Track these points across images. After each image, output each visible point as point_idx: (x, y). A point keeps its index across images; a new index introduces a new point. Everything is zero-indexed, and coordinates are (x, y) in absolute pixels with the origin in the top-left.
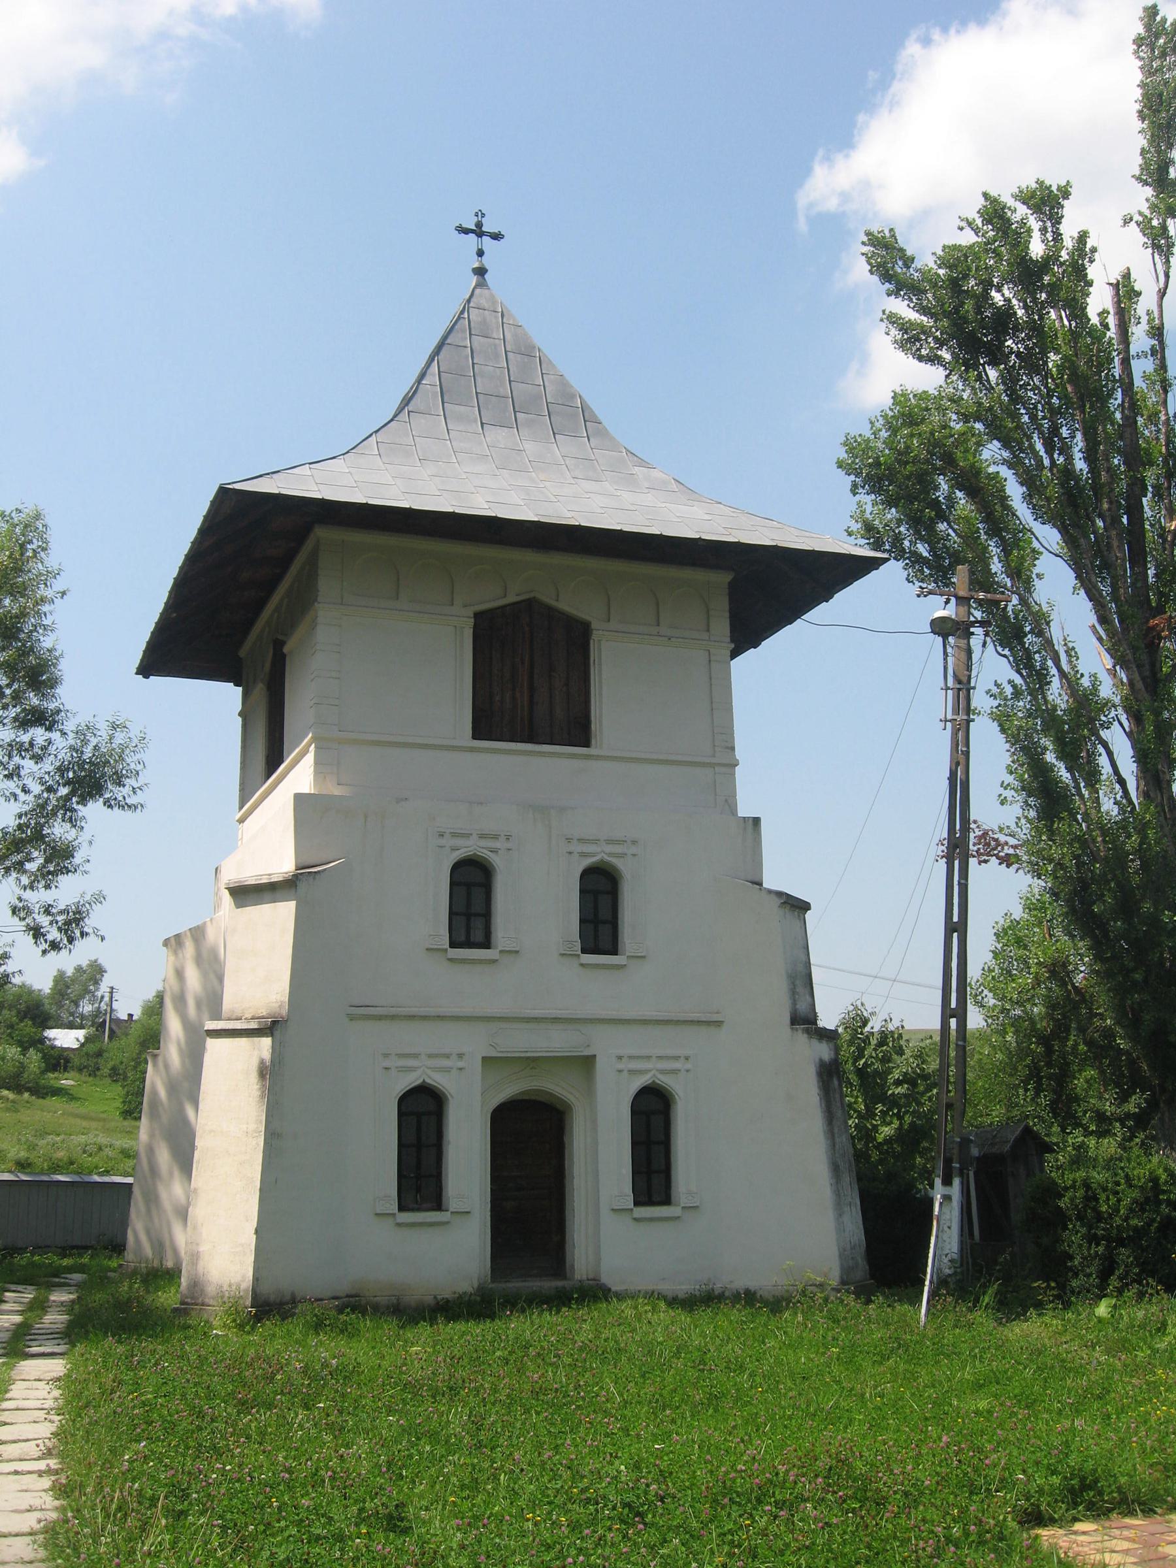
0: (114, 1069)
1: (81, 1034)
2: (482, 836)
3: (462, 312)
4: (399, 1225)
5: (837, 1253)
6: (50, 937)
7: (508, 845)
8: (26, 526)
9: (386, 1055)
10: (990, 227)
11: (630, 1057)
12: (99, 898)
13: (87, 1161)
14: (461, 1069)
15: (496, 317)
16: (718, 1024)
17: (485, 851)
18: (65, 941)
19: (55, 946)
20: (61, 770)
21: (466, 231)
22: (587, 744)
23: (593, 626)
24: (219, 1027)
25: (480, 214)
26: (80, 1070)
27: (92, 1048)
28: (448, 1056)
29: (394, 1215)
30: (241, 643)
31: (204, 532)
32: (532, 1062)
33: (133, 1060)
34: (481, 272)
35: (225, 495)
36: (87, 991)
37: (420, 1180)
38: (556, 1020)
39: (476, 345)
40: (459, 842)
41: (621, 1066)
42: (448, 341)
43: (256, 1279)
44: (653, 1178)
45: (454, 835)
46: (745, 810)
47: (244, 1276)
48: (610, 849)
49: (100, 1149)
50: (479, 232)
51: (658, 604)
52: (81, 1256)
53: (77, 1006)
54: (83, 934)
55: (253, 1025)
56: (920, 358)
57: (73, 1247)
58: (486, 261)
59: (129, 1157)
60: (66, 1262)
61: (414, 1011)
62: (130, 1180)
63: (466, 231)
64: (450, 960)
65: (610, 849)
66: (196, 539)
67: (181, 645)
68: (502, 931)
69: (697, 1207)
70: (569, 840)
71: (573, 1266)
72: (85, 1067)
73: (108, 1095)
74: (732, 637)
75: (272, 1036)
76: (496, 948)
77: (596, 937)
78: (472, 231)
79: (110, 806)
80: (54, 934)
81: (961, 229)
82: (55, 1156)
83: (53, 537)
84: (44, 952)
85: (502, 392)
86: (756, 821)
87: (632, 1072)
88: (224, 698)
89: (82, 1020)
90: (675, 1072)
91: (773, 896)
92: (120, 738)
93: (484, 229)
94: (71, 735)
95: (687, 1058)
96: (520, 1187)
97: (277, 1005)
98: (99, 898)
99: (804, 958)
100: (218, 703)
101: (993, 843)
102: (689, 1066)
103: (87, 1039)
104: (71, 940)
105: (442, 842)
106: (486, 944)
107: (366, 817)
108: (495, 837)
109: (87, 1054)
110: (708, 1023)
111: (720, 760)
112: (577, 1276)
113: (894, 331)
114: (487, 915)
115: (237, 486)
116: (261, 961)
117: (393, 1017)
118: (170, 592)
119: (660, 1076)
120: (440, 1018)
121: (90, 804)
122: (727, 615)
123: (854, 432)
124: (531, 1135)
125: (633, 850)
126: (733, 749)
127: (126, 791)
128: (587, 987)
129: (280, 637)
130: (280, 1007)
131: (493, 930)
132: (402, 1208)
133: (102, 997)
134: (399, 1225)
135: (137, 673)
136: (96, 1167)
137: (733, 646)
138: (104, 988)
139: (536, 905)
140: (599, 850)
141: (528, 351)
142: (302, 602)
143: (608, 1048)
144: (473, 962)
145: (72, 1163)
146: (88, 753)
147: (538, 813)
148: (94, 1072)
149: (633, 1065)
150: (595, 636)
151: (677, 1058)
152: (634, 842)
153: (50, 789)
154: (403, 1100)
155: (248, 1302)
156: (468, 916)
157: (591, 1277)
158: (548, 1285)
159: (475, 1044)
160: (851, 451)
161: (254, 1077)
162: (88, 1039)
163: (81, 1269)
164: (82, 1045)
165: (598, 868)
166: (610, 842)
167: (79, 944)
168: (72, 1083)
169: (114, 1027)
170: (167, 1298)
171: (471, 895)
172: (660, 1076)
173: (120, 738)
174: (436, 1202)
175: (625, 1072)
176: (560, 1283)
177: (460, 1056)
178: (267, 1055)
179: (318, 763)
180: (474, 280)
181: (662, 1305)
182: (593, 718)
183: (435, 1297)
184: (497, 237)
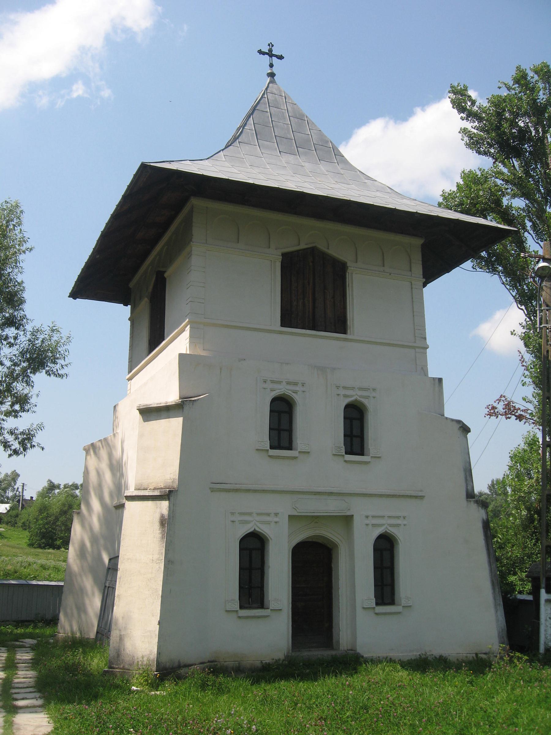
0: (23, 523)
1: (8, 506)
2: (288, 383)
3: (264, 94)
4: (240, 617)
5: (497, 634)
6: (13, 448)
7: (304, 389)
8: (11, 210)
9: (233, 514)
10: (517, 85)
11: (389, 517)
12: (41, 427)
13: (26, 571)
14: (276, 522)
15: (282, 99)
16: (421, 497)
17: (290, 392)
18: (22, 450)
19: (16, 452)
20: (22, 353)
22: (345, 332)
23: (348, 265)
24: (141, 494)
25: (271, 45)
26: (7, 523)
27: (14, 513)
28: (268, 515)
29: (237, 611)
30: (130, 280)
31: (125, 198)
32: (315, 519)
33: (35, 519)
34: (272, 75)
36: (10, 485)
37: (252, 591)
38: (331, 494)
39: (272, 112)
40: (276, 386)
41: (367, 522)
42: (257, 108)
43: (159, 653)
44: (385, 589)
45: (273, 382)
46: (433, 373)
47: (151, 651)
48: (360, 393)
49: (30, 565)
50: (270, 54)
52: (27, 627)
53: (5, 492)
54: (33, 446)
55: (157, 493)
56: (479, 153)
57: (23, 621)
58: (274, 70)
59: (45, 569)
60: (20, 631)
61: (250, 487)
62: (62, 584)
63: (263, 53)
64: (270, 456)
65: (360, 393)
66: (120, 202)
67: (100, 279)
69: (410, 606)
70: (338, 387)
71: (338, 642)
72: (10, 522)
73: (21, 536)
74: (423, 274)
75: (169, 500)
76: (297, 450)
77: (352, 445)
78: (266, 54)
79: (50, 375)
80: (16, 445)
81: (500, 88)
82: (6, 568)
83: (25, 218)
84: (10, 455)
85: (289, 136)
86: (440, 380)
87: (373, 525)
88: (122, 312)
89: (8, 499)
90: (398, 525)
92: (55, 338)
94: (28, 333)
95: (404, 518)
96: (303, 592)
97: (171, 481)
98: (41, 427)
99: (468, 460)
100: (114, 319)
101: (512, 409)
102: (405, 522)
103: (11, 508)
104: (25, 449)
105: (265, 386)
106: (290, 447)
107: (221, 369)
108: (296, 384)
109: (11, 516)
110: (416, 497)
111: (418, 345)
112: (341, 648)
113: (466, 139)
114: (290, 431)
115: (152, 164)
116: (154, 455)
117: (236, 490)
118: (98, 241)
119: (390, 528)
120: (264, 491)
121: (37, 374)
122: (421, 262)
123: (447, 190)
124: (315, 562)
126: (425, 339)
127: (58, 366)
128: (347, 475)
129: (162, 269)
130: (173, 482)
131: (294, 439)
132: (241, 607)
133: (18, 488)
134: (240, 617)
136: (29, 575)
137: (424, 280)
138: (19, 484)
139: (319, 425)
140: (354, 393)
141: (301, 117)
142: (181, 243)
143: (360, 510)
144: (284, 458)
145: (16, 572)
146: (38, 342)
148: (14, 524)
149: (375, 521)
150: (349, 271)
151: (398, 517)
152: (374, 390)
153: (15, 364)
154: (243, 540)
155: (154, 668)
157: (349, 648)
158: (326, 654)
159: (284, 507)
160: (445, 198)
161: (157, 525)
162: (12, 508)
163: (31, 636)
164: (8, 511)
165: (355, 406)
166: (361, 389)
167: (30, 452)
168: (3, 530)
169: (24, 503)
170: (96, 663)
171: (282, 418)
172: (390, 528)
173: (55, 338)
174: (261, 603)
176: (333, 653)
177: (276, 514)
178: (165, 512)
179: (191, 336)
180: (268, 80)
181: (399, 667)
182: (348, 318)
183: (262, 662)
184: (281, 57)
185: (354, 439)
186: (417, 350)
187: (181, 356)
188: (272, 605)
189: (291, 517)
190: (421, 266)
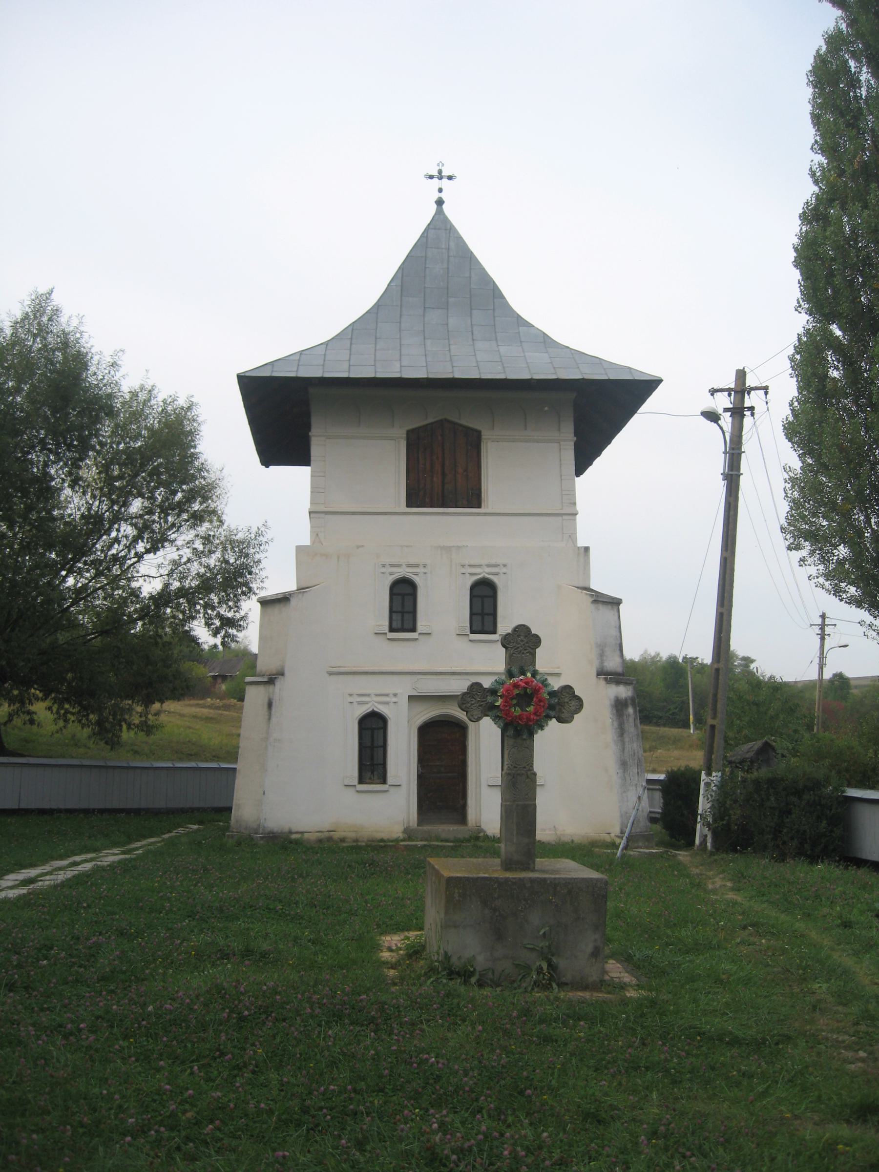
2: (409, 566)
21: (431, 177)
22: (479, 506)
28: (387, 695)
29: (355, 786)
37: (372, 765)
38: (454, 674)
45: (392, 566)
48: (488, 570)
55: (266, 679)
58: (443, 195)
63: (431, 177)
65: (488, 570)
68: (422, 624)
86: (587, 549)
99: (614, 633)
106: (413, 629)
107: (338, 558)
108: (417, 566)
114: (414, 612)
115: (247, 374)
125: (504, 570)
126: (575, 504)
132: (361, 781)
147: (444, 548)
152: (505, 566)
156: (403, 613)
159: (404, 688)
166: (488, 566)
171: (403, 603)
177: (395, 695)
184: (450, 178)
185: (486, 617)
186: (565, 517)
187: (300, 549)
188: (390, 780)
189: (411, 698)
190: (573, 423)
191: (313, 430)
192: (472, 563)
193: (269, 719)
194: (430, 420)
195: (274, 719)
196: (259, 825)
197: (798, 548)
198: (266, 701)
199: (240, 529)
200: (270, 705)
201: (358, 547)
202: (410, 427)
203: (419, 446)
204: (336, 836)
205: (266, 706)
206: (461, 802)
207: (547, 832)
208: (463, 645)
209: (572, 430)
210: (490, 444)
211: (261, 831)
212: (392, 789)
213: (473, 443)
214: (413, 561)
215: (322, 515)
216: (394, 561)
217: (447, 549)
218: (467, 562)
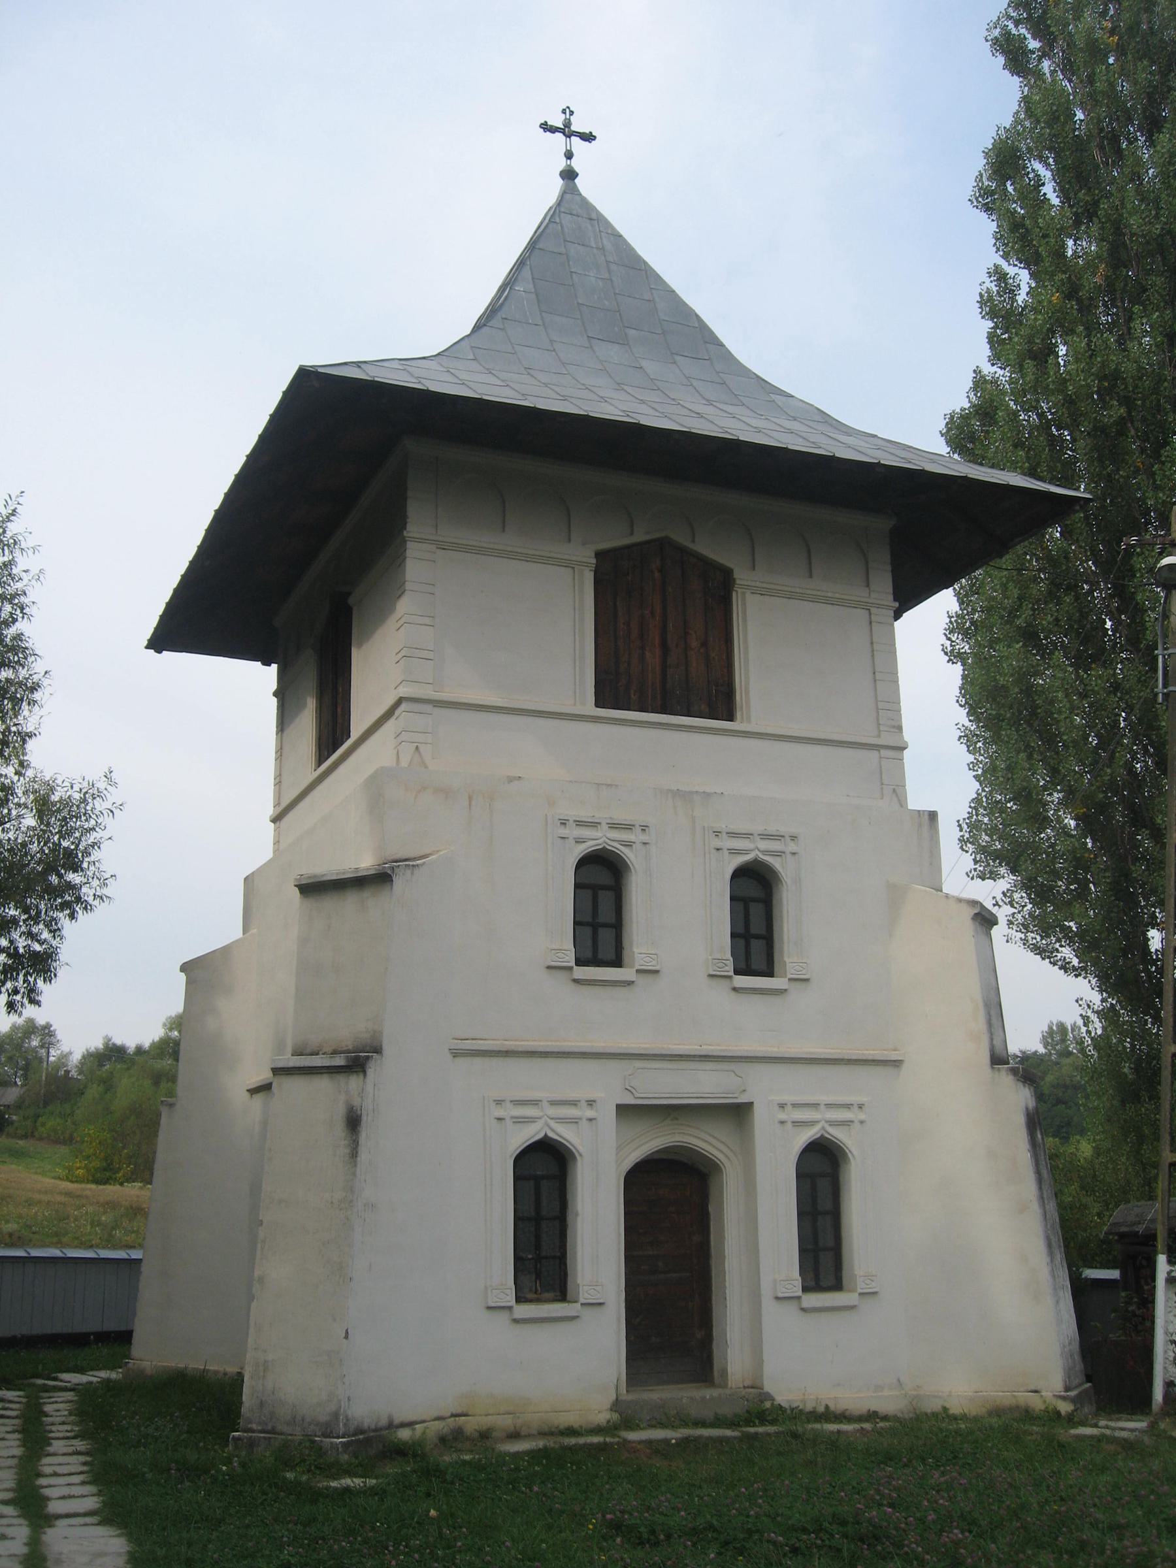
2: (614, 826)
9: (499, 1102)
11: (794, 1105)
28: (574, 1103)
29: (510, 1308)
35: (306, 378)
37: (542, 1264)
41: (782, 1116)
44: (823, 1257)
45: (580, 823)
48: (764, 845)
50: (567, 131)
51: (809, 552)
55: (339, 1061)
58: (575, 164)
64: (576, 981)
65: (764, 845)
67: (201, 617)
74: (894, 594)
76: (633, 967)
86: (933, 816)
87: (797, 1124)
88: (255, 681)
90: (847, 1123)
91: (964, 906)
93: (573, 128)
95: (860, 1107)
100: (242, 690)
107: (470, 798)
108: (629, 827)
114: (617, 926)
115: (320, 370)
119: (831, 1130)
122: (889, 568)
124: (673, 1200)
125: (792, 847)
126: (900, 728)
128: (740, 1020)
132: (519, 1299)
135: (147, 647)
139: (677, 914)
140: (751, 846)
143: (765, 1092)
149: (799, 1115)
152: (793, 838)
156: (595, 926)
159: (607, 1088)
175: (789, 1125)
177: (591, 1103)
184: (588, 137)
186: (884, 753)
191: (409, 527)
192: (733, 827)
193: (354, 1154)
194: (640, 537)
195: (363, 1156)
196: (336, 1415)
197: (994, 876)
198: (340, 1111)
199: (59, 782)
200: (353, 1122)
201: (511, 779)
202: (602, 546)
203: (620, 587)
204: (471, 1425)
205: (340, 1129)
206: (699, 1335)
207: (886, 1393)
208: (719, 998)
209: (891, 590)
210: (752, 601)
211: (342, 1430)
212: (586, 1314)
213: (718, 591)
214: (621, 816)
215: (428, 708)
216: (585, 814)
217: (684, 796)
218: (722, 826)
